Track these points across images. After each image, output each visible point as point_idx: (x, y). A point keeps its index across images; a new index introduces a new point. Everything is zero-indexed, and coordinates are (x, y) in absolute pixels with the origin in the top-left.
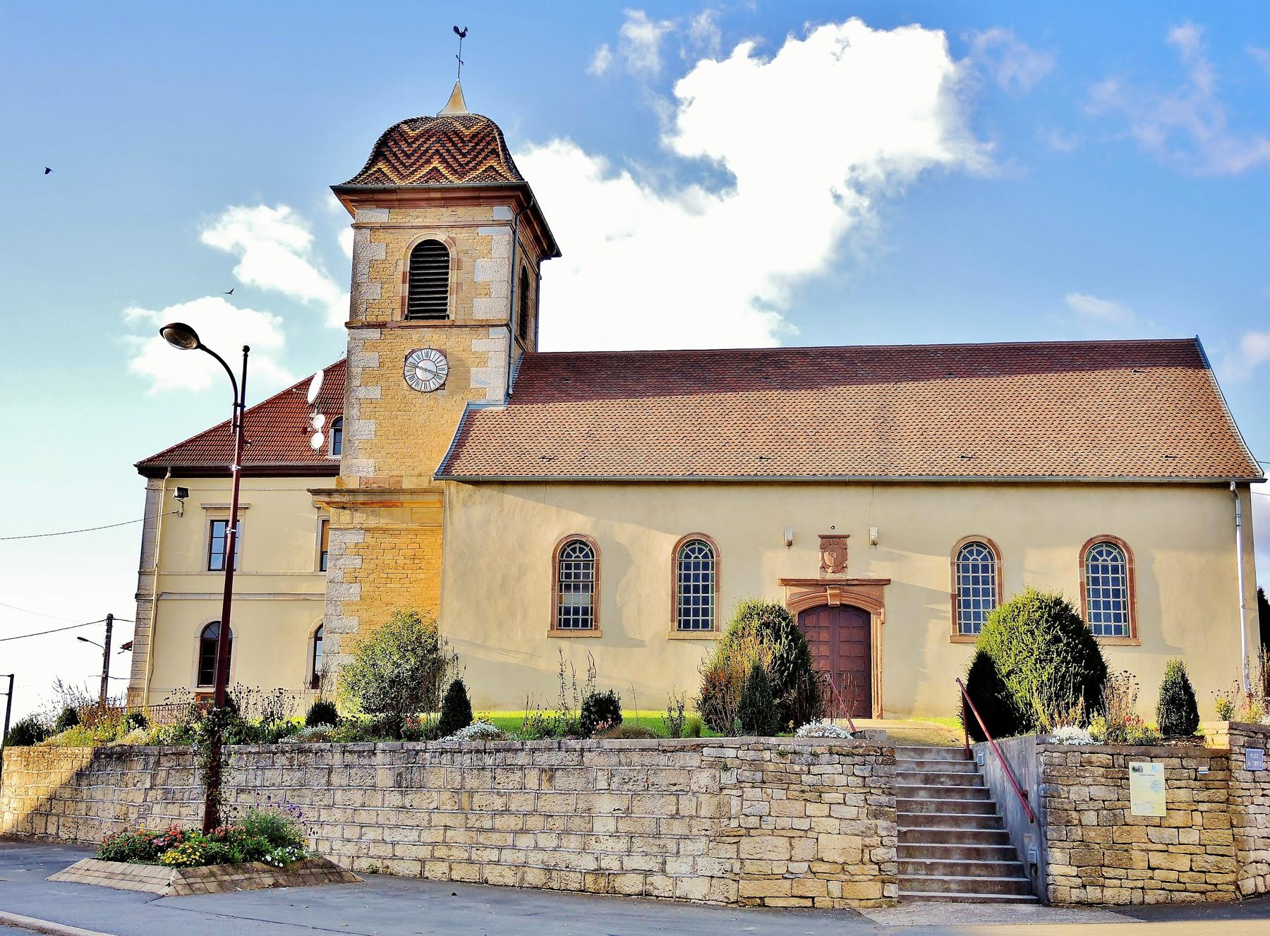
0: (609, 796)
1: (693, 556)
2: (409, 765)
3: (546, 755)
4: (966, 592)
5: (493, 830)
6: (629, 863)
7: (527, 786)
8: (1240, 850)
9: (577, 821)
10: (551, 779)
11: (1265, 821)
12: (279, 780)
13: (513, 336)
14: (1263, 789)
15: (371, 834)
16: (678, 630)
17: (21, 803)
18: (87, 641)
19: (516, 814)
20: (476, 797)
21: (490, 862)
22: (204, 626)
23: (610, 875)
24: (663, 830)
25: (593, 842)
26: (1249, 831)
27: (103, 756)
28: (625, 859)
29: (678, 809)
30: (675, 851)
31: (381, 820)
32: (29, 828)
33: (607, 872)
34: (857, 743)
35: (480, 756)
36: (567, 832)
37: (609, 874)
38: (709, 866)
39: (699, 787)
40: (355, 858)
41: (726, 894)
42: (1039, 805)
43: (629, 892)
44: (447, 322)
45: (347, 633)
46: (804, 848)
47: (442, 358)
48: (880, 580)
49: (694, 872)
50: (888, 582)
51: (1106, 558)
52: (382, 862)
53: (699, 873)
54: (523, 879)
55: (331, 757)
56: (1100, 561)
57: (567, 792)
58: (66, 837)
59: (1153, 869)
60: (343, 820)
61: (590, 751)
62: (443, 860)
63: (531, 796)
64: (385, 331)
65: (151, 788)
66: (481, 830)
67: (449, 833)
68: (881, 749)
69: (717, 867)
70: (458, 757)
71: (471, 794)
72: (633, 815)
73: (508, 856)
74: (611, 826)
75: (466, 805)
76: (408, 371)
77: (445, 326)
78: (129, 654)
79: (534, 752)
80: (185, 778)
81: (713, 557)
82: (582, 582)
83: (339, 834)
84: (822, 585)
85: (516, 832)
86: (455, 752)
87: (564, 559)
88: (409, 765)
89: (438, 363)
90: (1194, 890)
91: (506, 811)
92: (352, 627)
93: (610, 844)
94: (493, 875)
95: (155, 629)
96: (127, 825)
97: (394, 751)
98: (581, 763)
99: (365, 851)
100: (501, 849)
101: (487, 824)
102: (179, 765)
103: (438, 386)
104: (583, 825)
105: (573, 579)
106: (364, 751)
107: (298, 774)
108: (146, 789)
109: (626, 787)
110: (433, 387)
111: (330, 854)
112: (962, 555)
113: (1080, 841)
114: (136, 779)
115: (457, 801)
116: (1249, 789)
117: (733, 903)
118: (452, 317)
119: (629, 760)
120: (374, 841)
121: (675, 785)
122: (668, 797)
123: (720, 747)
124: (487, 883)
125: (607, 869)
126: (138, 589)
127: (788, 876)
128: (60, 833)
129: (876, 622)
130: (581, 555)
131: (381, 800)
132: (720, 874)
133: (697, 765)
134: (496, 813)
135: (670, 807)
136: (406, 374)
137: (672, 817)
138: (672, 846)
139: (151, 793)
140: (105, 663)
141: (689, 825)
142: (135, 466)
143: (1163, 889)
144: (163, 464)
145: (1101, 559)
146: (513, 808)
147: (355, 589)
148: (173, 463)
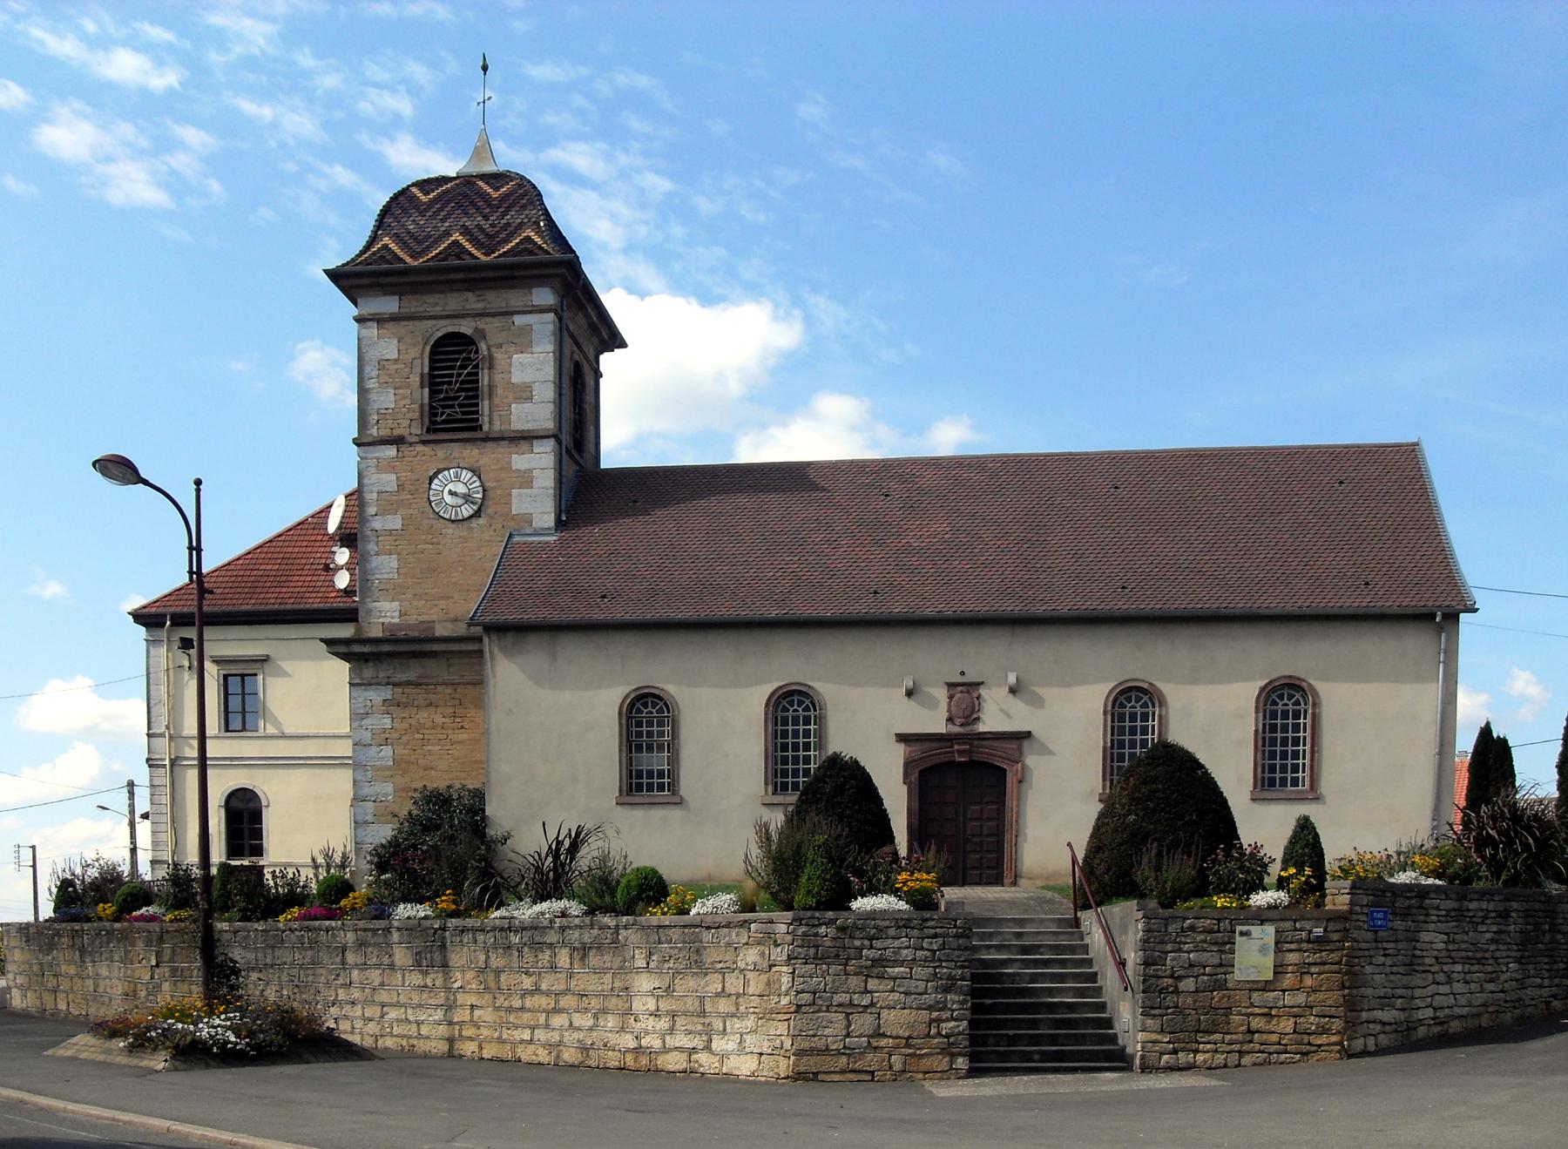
0: (648, 975)
1: (792, 709)
2: (428, 944)
3: (577, 933)
4: (1121, 744)
5: (522, 1009)
6: (670, 1042)
7: (558, 965)
8: (1351, 1011)
9: (614, 1000)
10: (583, 959)
11: (1383, 981)
12: (290, 958)
13: (564, 449)
14: (1385, 949)
15: (393, 1014)
16: (773, 794)
17: (28, 979)
18: (108, 809)
19: (548, 993)
20: (503, 977)
21: (522, 1041)
22: (1254, 699)
23: (650, 1053)
24: (708, 1008)
25: (632, 1020)
26: (1363, 991)
27: (104, 933)
28: (668, 1038)
29: (723, 987)
30: (721, 1029)
31: (402, 999)
32: (38, 1003)
33: (648, 1051)
34: (928, 915)
35: (504, 934)
36: (604, 1011)
37: (651, 1053)
38: (753, 1042)
39: (747, 964)
40: (379, 1037)
41: (776, 1070)
42: (1135, 973)
43: (672, 1070)
44: (478, 434)
45: (381, 801)
46: (863, 1023)
47: (475, 478)
48: (1019, 733)
49: (741, 1050)
50: (1028, 735)
51: (1288, 702)
52: (408, 1041)
53: (747, 1050)
54: (558, 1057)
55: (343, 936)
56: (1280, 706)
57: (603, 971)
58: (77, 1013)
59: (1254, 1033)
60: (362, 999)
61: (626, 929)
62: (471, 1039)
63: (563, 976)
64: (403, 448)
65: (157, 965)
66: (510, 1010)
67: (477, 1013)
68: (956, 921)
69: (766, 1044)
70: (481, 937)
71: (498, 972)
72: (675, 994)
73: (541, 1035)
74: (651, 1005)
75: (492, 984)
76: (433, 495)
77: (476, 440)
78: (147, 823)
79: (564, 931)
80: (192, 955)
81: (815, 710)
82: (645, 741)
83: (359, 1013)
84: (948, 740)
85: (548, 1012)
86: (477, 930)
87: (634, 715)
88: (428, 944)
89: (470, 485)
90: (1294, 1051)
91: (537, 990)
92: (386, 795)
93: (651, 1023)
94: (526, 1054)
95: (173, 798)
96: (138, 1003)
97: (411, 929)
98: (615, 941)
99: (389, 1030)
100: (533, 1028)
101: (517, 1003)
102: (184, 942)
103: (471, 512)
104: (620, 1004)
105: (645, 738)
106: (379, 929)
107: (310, 953)
108: (152, 966)
109: (666, 965)
110: (466, 514)
111: (352, 1033)
112: (1118, 702)
113: (1174, 1007)
114: (141, 957)
115: (482, 980)
116: (1368, 950)
117: (782, 1078)
118: (486, 428)
119: (669, 938)
120: (398, 1020)
121: (720, 962)
122: (713, 975)
123: (769, 922)
124: (520, 1061)
125: (648, 1048)
126: (149, 753)
127: (847, 1051)
128: (71, 1010)
129: (1012, 780)
130: (800, 709)
131: (400, 979)
132: (770, 1051)
133: (744, 941)
134: (525, 994)
135: (716, 986)
136: (432, 499)
137: (718, 995)
138: (718, 1025)
139: (157, 971)
140: (131, 832)
141: (736, 1003)
142: (129, 613)
143: (1263, 1052)
144: (161, 610)
145: (1281, 703)
146: (544, 987)
147: (387, 751)
148: (172, 610)
